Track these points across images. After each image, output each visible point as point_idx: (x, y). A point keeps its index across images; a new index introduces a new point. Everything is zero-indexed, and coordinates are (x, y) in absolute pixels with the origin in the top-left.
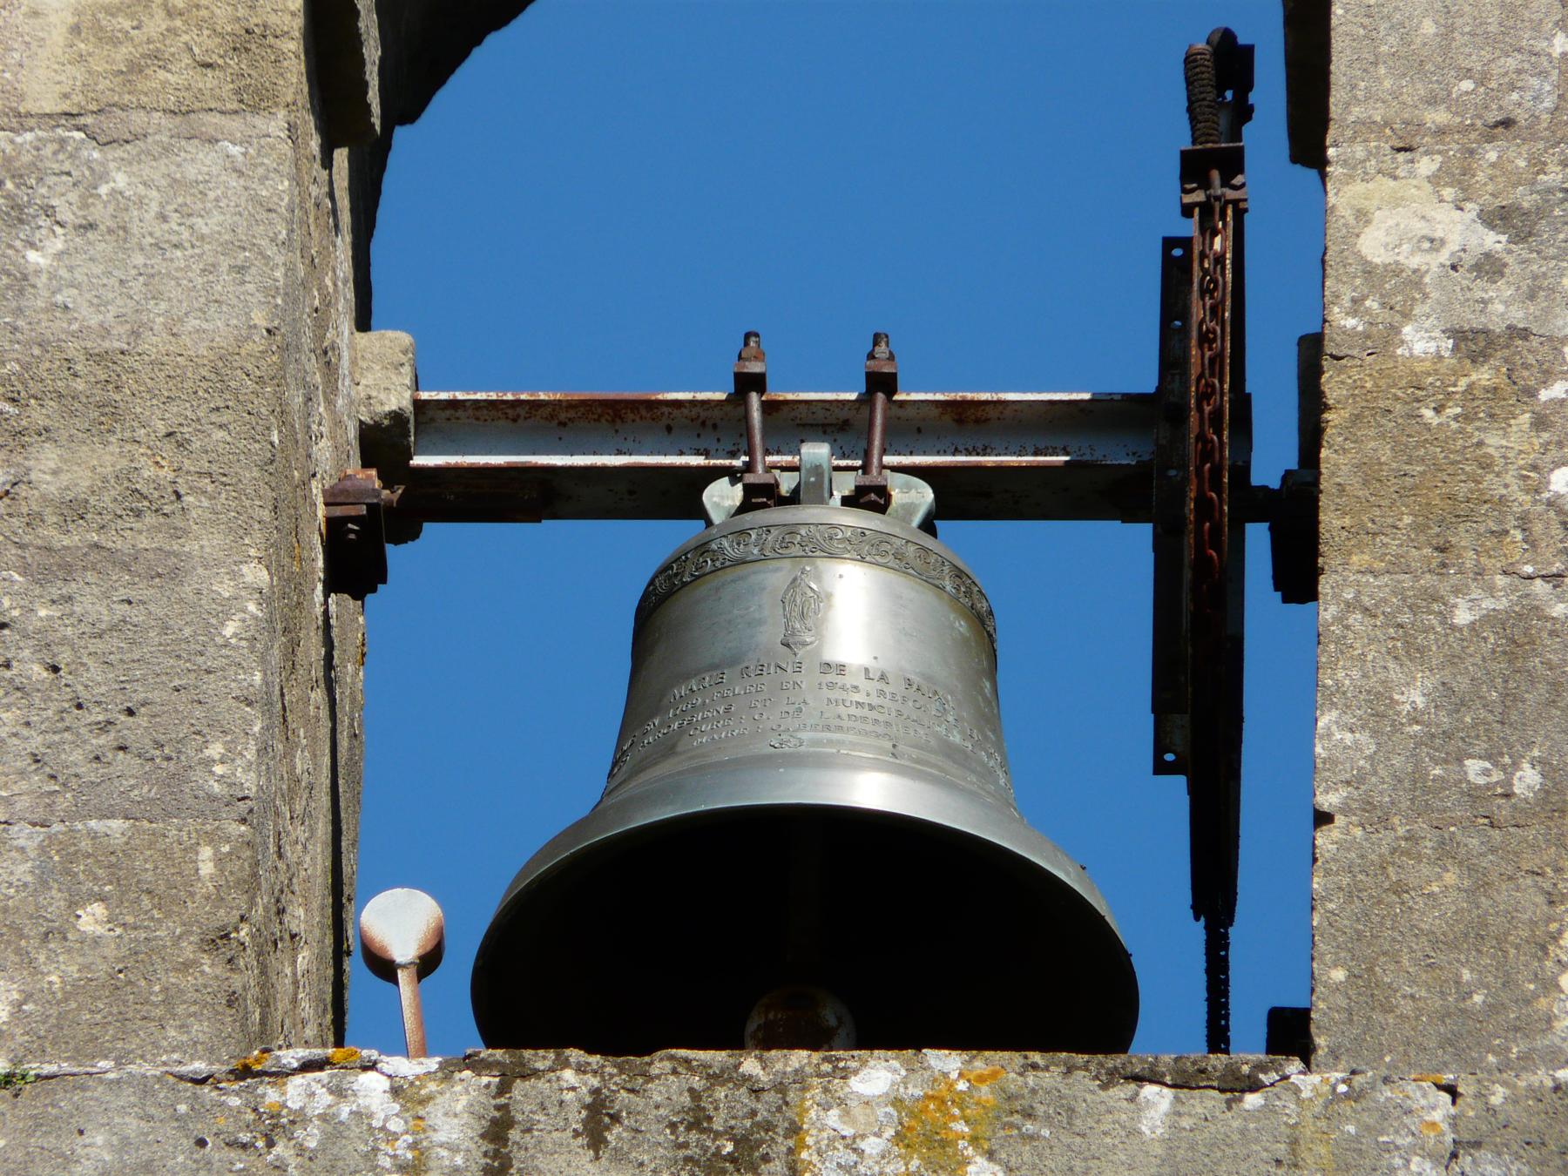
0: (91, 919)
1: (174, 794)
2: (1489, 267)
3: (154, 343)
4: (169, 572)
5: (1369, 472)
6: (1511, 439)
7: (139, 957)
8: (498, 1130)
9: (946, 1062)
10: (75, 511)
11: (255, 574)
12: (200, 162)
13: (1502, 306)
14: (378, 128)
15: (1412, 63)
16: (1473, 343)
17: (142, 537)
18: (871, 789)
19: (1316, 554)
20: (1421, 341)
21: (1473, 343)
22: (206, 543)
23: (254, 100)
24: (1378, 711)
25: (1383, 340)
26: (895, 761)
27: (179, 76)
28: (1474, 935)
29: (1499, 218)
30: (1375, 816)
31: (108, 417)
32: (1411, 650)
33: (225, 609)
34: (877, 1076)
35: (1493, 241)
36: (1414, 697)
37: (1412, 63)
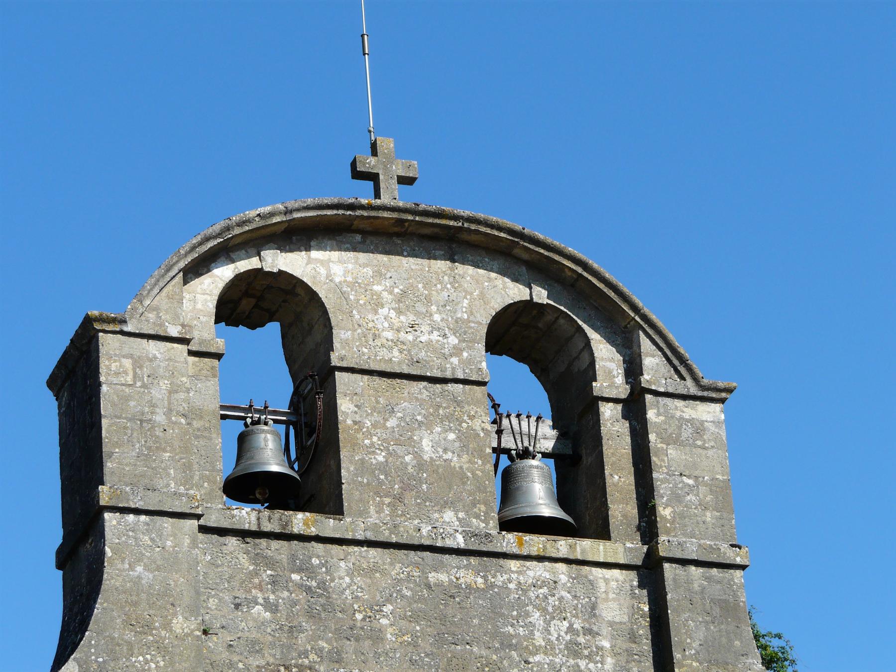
0: (206, 484)
1: (214, 470)
2: (356, 413)
3: (205, 408)
4: (210, 439)
5: (345, 438)
6: (360, 436)
7: (212, 490)
8: (258, 519)
9: (308, 514)
10: (199, 430)
11: (220, 440)
12: (209, 384)
13: (358, 419)
14: (572, 522)
15: (345, 385)
16: (355, 423)
17: (206, 434)
18: (275, 468)
19: (665, 588)
20: (349, 422)
21: (355, 423)
22: (214, 436)
23: (214, 376)
24: (348, 470)
25: (345, 421)
26: (278, 464)
27: (205, 372)
28: (361, 500)
29: (356, 406)
30: (349, 484)
31: (201, 418)
32: (351, 463)
33: (217, 445)
34: (300, 515)
35: (356, 409)
36: (352, 469)
37: (345, 385)
